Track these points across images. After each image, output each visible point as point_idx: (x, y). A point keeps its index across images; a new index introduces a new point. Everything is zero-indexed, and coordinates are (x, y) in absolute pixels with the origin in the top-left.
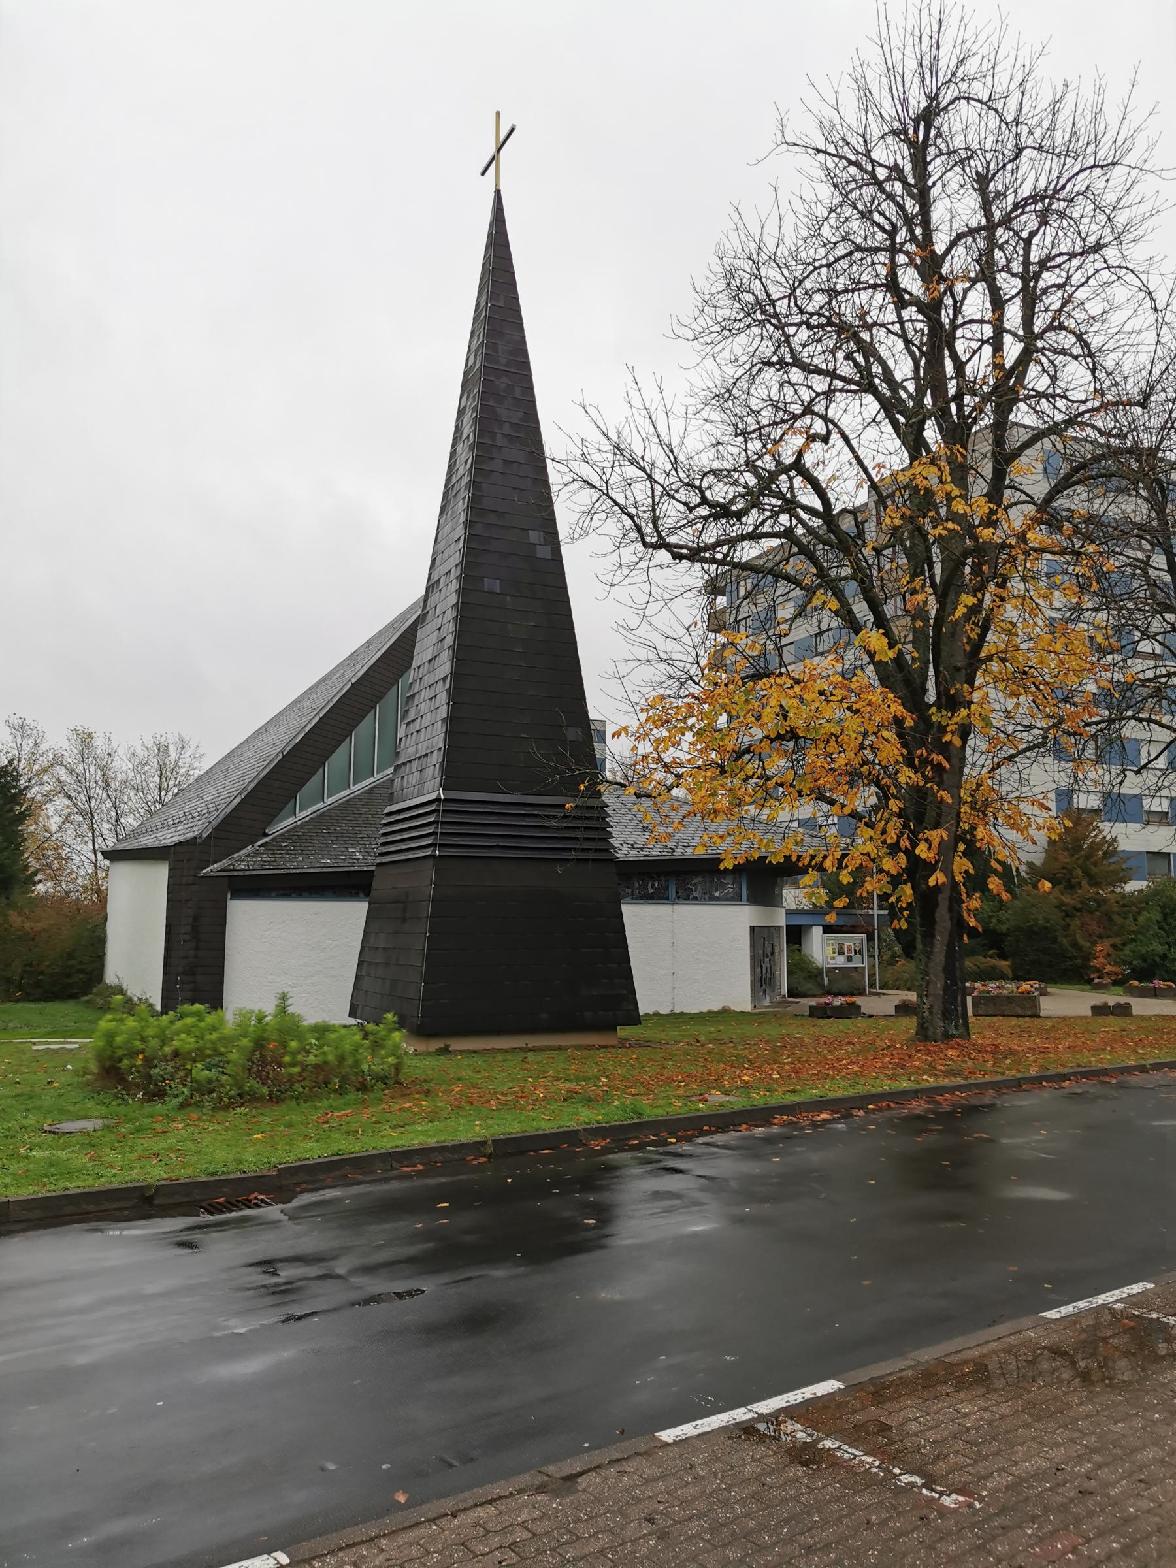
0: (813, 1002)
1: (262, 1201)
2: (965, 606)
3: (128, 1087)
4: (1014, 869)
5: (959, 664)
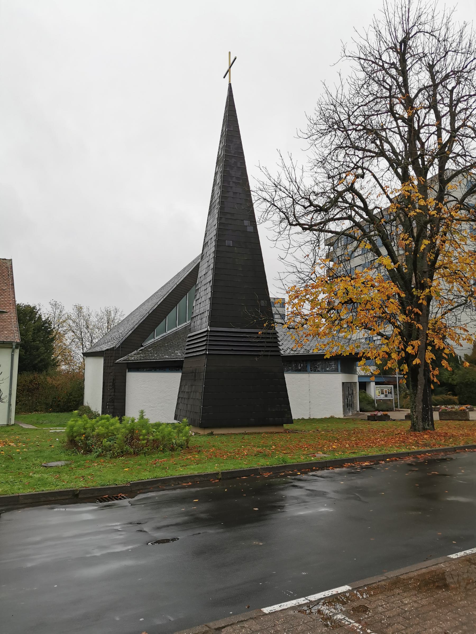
0: (369, 414)
1: (123, 497)
2: (425, 245)
3: (78, 448)
4: (459, 357)
5: (425, 270)
